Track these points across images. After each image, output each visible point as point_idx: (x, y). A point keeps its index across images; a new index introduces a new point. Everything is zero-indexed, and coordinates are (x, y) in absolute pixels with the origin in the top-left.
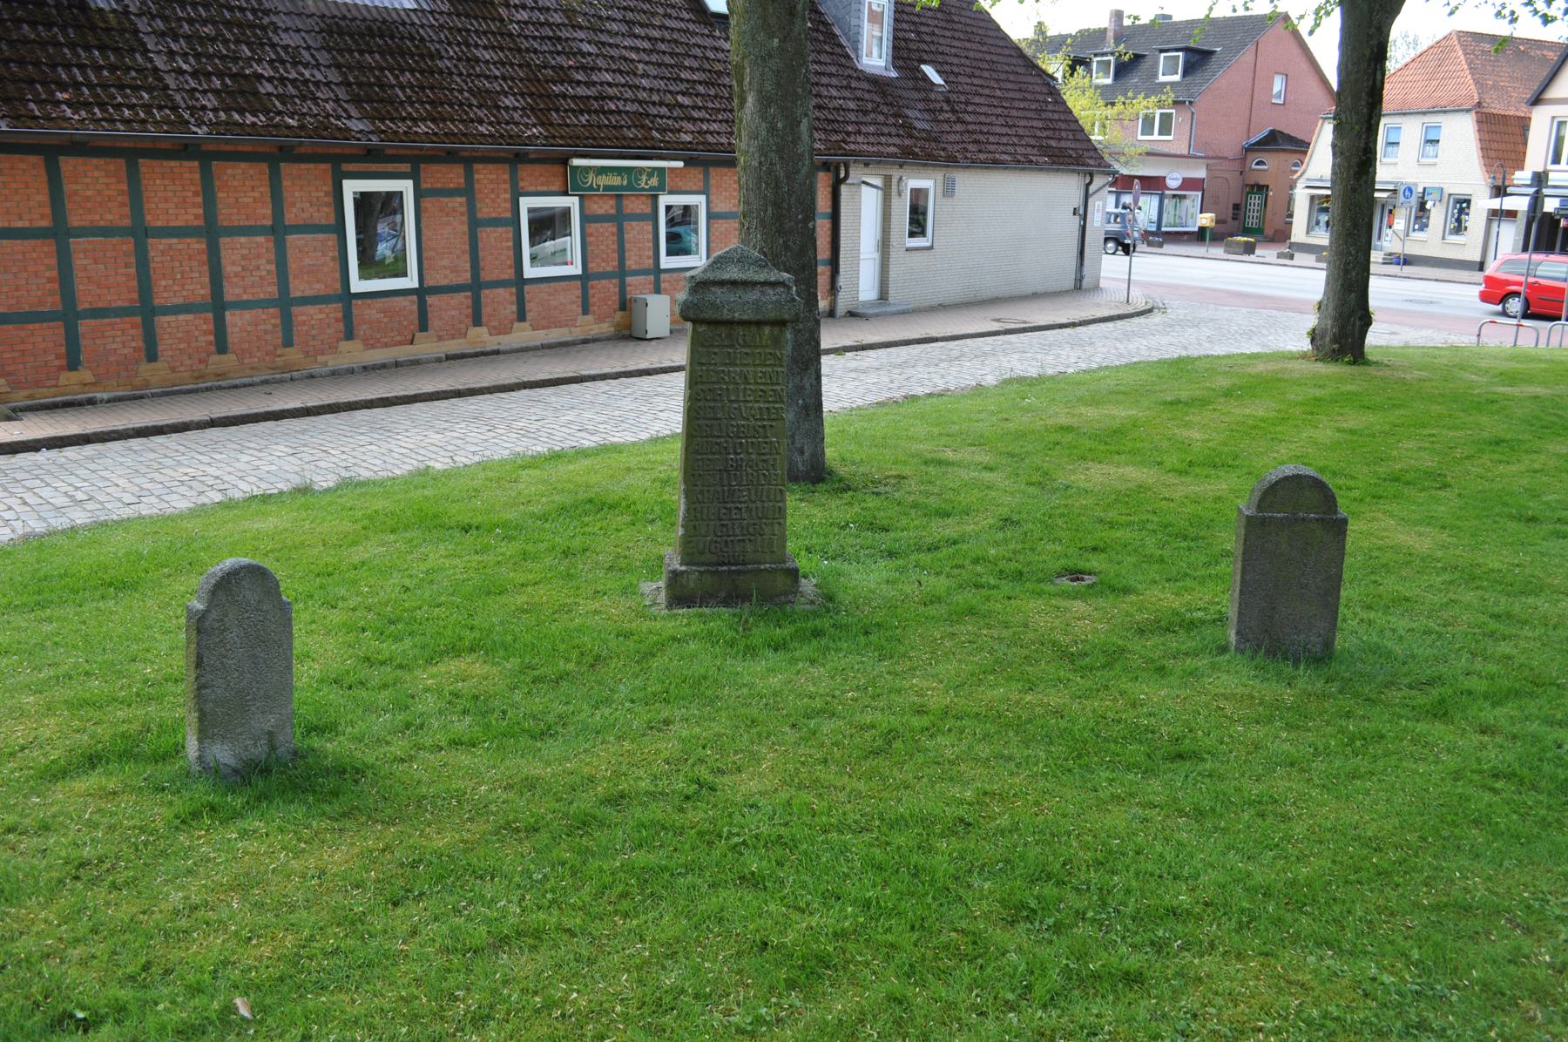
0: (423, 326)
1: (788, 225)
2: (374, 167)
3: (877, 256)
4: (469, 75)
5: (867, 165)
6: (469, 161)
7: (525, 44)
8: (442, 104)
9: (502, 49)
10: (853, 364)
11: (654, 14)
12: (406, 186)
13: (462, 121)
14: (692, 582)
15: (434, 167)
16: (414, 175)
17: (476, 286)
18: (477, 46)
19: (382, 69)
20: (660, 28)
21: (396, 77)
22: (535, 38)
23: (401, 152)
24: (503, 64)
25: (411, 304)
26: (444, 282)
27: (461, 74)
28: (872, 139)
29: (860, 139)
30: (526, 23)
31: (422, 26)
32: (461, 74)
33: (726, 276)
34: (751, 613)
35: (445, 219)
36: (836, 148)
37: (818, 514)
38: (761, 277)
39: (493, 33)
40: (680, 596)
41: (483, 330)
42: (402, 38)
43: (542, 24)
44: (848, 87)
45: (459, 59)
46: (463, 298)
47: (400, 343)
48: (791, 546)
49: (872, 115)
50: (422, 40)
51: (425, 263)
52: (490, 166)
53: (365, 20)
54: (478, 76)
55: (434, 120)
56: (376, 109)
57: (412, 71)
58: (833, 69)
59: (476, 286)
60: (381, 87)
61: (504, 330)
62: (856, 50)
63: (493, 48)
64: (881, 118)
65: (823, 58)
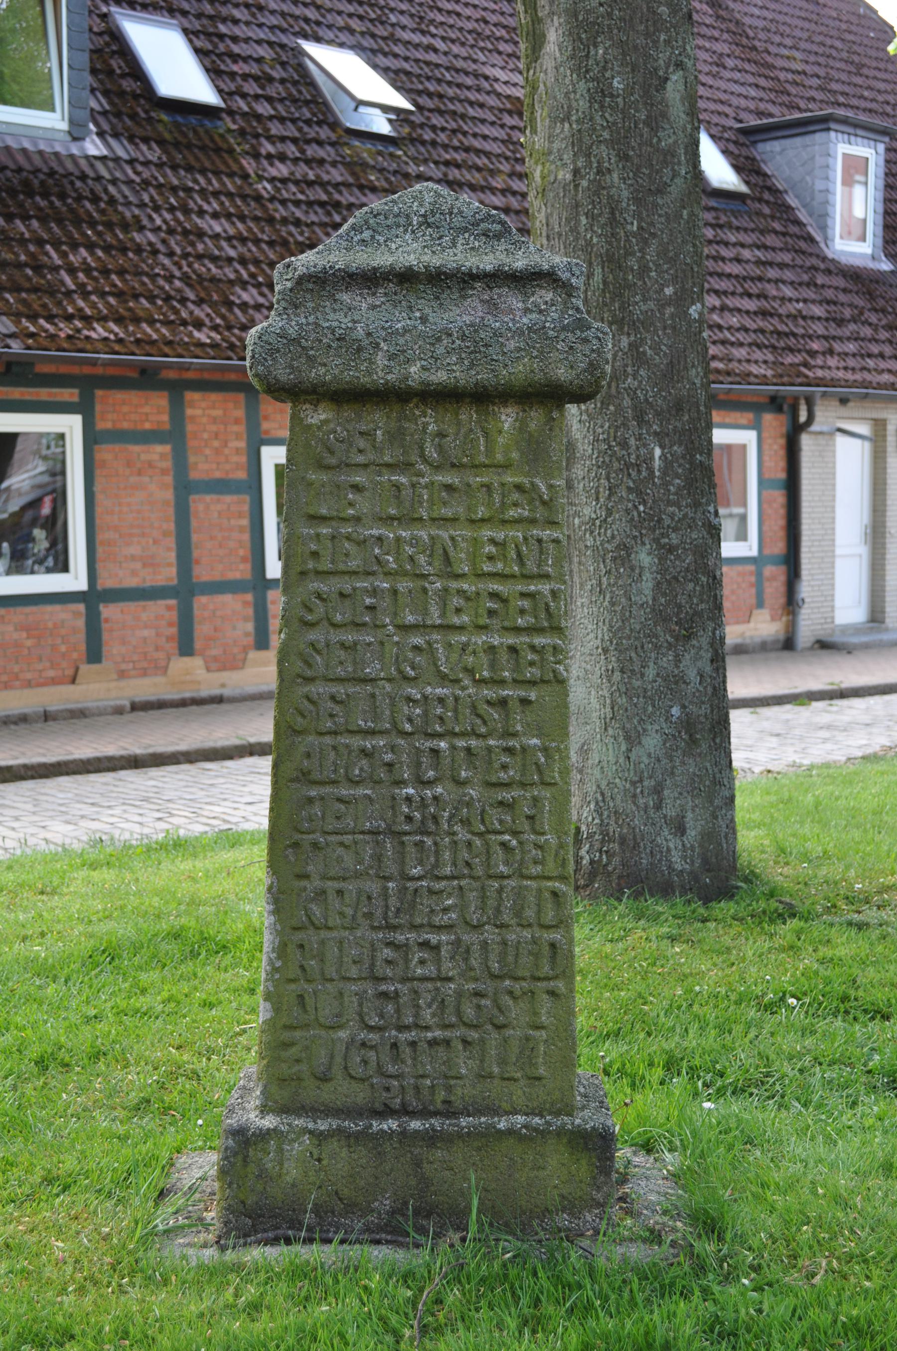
0: (94, 654)
1: (640, 308)
2: (16, 393)
3: (863, 551)
4: (186, 256)
5: (844, 401)
6: (178, 389)
7: (281, 212)
8: (136, 297)
9: (242, 218)
10: (825, 719)
11: (493, 173)
12: (71, 425)
13: (167, 323)
14: (292, 1166)
15: (119, 395)
16: (84, 408)
17: (185, 591)
18: (201, 213)
19: (40, 242)
20: (503, 192)
21: (64, 255)
22: (297, 203)
23: (64, 369)
24: (243, 240)
25: (73, 618)
26: (131, 582)
27: (171, 254)
28: (851, 362)
29: (832, 362)
30: (284, 181)
31: (114, 182)
32: (171, 254)
33: (382, 259)
34: (458, 1273)
35: (133, 479)
36: (793, 374)
37: (711, 976)
38: (487, 262)
39: (229, 195)
40: (257, 1213)
41: (195, 663)
42: (79, 198)
43: (310, 184)
44: (811, 284)
45: (171, 232)
46: (162, 611)
47: (54, 682)
48: (591, 1059)
49: (852, 327)
50: (112, 201)
51: (100, 551)
52: (214, 396)
53: (20, 170)
54: (200, 257)
55: (119, 320)
56: (24, 302)
57: (91, 247)
58: (786, 257)
59: (185, 591)
60: (38, 268)
61: (230, 662)
62: (824, 228)
63: (229, 216)
64: (867, 331)
65: (771, 240)
